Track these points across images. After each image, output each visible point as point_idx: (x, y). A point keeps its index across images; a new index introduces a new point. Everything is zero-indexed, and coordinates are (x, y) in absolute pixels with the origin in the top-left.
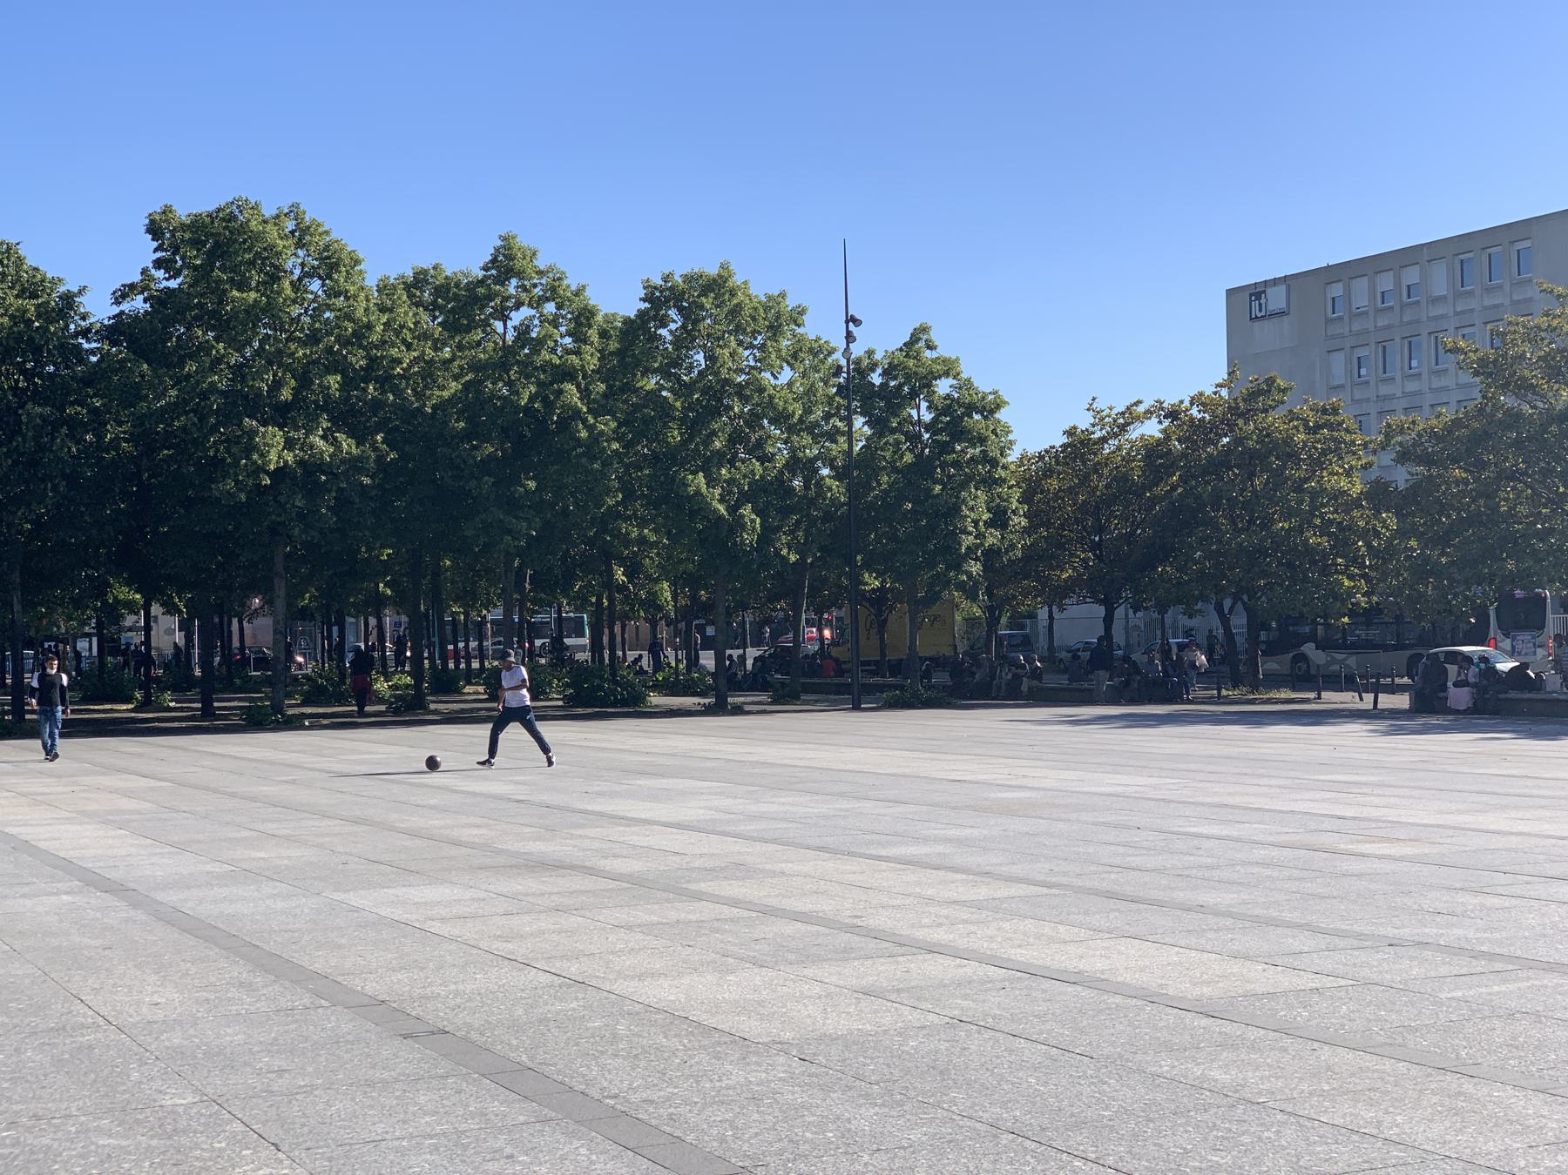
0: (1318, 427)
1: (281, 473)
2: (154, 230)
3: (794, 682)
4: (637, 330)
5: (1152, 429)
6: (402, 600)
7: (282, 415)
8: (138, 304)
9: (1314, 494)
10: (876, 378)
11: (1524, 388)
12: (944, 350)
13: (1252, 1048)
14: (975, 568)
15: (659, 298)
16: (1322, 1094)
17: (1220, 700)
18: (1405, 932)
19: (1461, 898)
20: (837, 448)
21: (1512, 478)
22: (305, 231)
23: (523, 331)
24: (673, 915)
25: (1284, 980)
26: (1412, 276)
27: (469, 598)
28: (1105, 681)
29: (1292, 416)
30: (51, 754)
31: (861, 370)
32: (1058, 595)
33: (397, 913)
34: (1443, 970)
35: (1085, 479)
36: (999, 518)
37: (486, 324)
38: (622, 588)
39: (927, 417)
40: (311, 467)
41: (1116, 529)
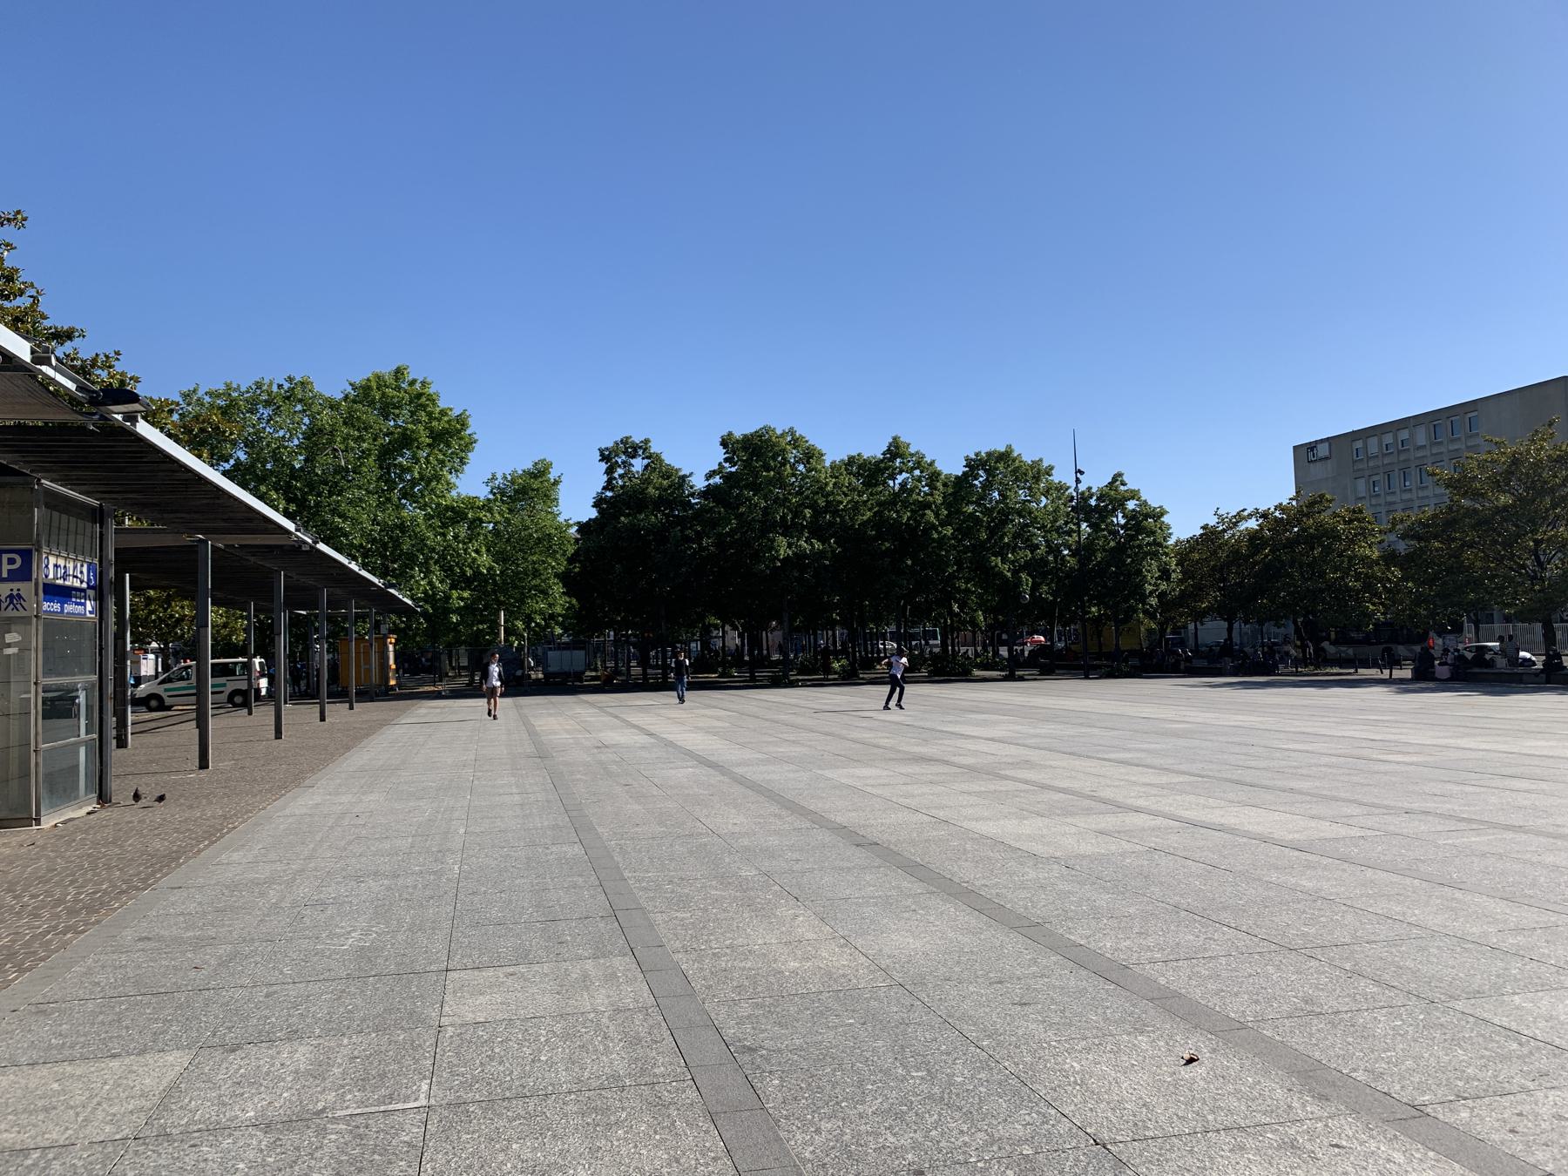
0: (1351, 521)
1: (787, 558)
2: (724, 443)
3: (1050, 665)
4: (962, 482)
5: (1253, 524)
6: (845, 623)
7: (788, 530)
8: (717, 480)
9: (1350, 558)
10: (1093, 502)
11: (1477, 495)
12: (1131, 486)
13: (1325, 868)
14: (1154, 601)
15: (973, 465)
16: (1368, 896)
17: (1297, 674)
18: (1415, 806)
19: (1449, 786)
20: (1072, 540)
21: (1471, 546)
22: (796, 440)
23: (903, 484)
24: (992, 787)
25: (1343, 831)
26: (1404, 435)
27: (878, 620)
28: (1229, 663)
29: (1335, 515)
30: (682, 700)
31: (1084, 498)
32: (1199, 616)
33: (849, 782)
34: (1439, 828)
35: (1215, 553)
36: (1165, 574)
37: (885, 483)
38: (958, 615)
39: (1122, 522)
40: (800, 556)
41: (1233, 579)
